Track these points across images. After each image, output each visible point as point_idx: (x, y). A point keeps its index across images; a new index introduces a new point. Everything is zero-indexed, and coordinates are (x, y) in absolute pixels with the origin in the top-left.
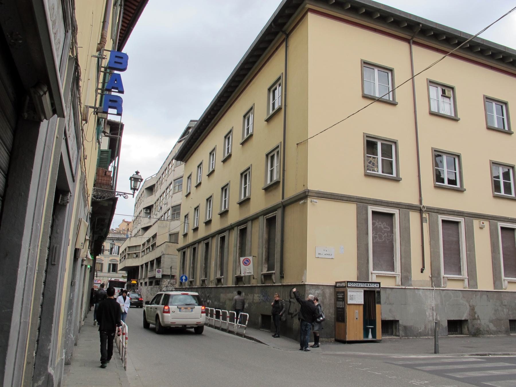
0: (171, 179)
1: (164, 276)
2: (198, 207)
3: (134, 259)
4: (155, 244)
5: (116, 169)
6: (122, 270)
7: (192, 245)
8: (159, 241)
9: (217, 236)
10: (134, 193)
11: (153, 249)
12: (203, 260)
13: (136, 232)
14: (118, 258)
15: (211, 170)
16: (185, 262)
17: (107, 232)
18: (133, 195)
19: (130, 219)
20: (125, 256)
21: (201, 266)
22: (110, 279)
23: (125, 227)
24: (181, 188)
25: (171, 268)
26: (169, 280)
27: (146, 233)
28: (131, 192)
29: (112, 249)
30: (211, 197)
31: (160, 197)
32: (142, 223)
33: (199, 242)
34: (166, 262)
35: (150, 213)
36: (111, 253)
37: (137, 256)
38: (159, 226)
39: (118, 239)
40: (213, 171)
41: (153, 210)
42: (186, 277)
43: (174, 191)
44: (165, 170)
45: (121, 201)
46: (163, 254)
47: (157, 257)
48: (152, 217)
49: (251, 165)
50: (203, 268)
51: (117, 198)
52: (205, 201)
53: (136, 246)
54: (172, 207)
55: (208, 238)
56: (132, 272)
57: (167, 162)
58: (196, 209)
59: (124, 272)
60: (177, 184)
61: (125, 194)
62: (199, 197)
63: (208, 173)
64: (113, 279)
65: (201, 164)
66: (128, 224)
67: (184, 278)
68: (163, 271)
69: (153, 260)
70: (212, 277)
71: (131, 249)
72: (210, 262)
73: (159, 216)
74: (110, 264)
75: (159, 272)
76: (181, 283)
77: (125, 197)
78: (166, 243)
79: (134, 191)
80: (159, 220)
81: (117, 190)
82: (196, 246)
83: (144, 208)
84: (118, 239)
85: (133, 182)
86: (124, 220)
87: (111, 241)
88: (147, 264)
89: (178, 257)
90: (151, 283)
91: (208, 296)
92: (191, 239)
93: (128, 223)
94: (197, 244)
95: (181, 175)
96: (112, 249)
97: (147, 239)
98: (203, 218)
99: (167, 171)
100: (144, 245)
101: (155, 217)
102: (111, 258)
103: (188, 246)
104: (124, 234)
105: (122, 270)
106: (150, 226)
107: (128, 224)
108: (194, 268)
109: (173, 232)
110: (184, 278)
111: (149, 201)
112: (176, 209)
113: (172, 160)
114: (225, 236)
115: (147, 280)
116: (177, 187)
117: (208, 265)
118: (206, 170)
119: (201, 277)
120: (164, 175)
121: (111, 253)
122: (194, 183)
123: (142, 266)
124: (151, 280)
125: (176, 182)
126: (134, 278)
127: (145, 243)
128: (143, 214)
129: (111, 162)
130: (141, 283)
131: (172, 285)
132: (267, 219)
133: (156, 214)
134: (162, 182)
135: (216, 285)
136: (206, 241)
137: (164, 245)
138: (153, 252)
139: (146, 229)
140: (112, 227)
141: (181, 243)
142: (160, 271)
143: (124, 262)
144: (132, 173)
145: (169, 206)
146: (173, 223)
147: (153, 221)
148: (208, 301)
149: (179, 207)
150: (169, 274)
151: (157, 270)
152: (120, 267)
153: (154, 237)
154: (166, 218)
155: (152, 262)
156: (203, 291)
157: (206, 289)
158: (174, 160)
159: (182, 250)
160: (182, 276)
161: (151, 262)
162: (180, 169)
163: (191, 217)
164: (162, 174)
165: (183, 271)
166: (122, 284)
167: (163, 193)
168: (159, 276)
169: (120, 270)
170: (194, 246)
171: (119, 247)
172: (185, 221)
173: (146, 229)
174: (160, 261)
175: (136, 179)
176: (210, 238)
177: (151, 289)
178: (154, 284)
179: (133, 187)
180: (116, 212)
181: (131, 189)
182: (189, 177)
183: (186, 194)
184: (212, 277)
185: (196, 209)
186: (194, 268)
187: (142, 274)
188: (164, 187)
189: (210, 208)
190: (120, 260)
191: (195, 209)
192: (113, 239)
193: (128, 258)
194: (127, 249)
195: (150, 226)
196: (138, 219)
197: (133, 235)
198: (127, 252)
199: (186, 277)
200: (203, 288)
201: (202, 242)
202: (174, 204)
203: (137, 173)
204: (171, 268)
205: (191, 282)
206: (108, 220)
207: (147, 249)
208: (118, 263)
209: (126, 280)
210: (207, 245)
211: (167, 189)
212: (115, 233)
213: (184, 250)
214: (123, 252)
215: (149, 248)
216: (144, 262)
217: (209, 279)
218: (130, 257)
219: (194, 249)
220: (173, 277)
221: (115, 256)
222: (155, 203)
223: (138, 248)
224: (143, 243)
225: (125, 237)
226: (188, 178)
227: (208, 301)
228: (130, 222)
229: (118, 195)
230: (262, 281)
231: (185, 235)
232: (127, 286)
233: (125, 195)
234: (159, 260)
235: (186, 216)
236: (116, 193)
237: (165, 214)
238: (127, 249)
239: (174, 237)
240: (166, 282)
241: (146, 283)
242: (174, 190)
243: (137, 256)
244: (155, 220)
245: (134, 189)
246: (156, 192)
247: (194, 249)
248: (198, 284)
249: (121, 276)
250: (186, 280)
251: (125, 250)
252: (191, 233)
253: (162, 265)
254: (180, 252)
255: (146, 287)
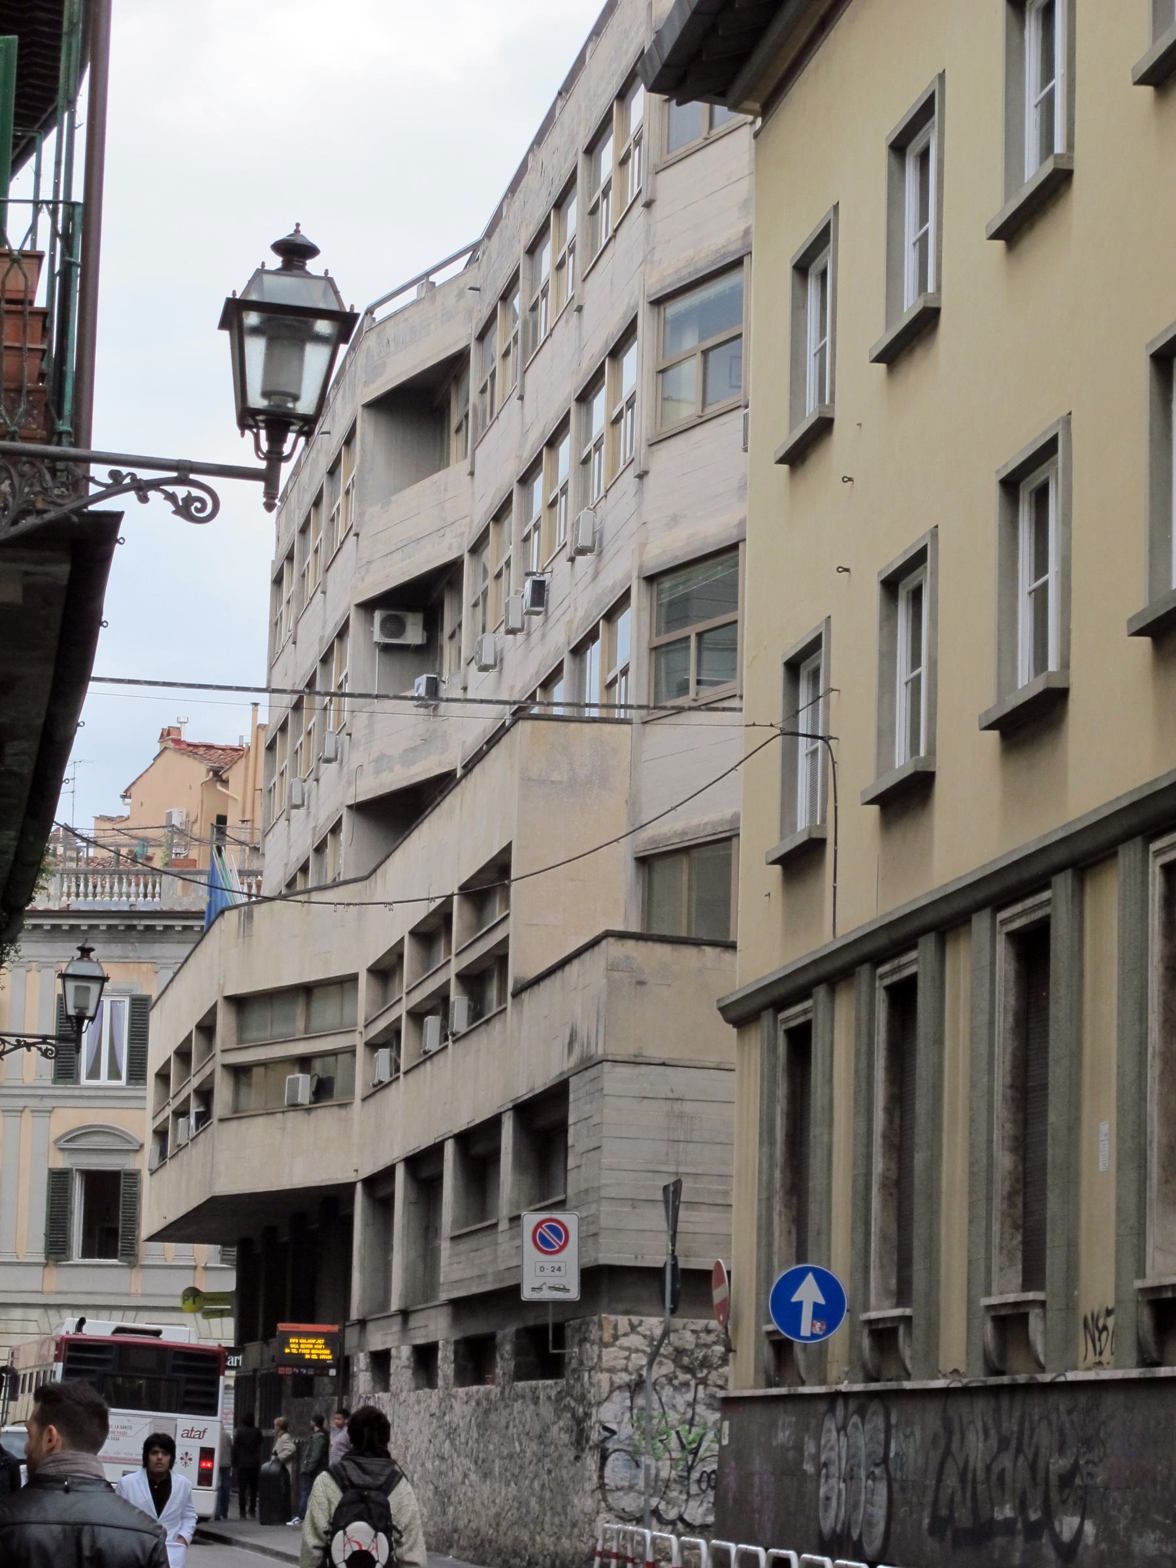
0: (617, 289)
1: (599, 1280)
2: (815, 645)
3: (295, 1119)
4: (499, 957)
5: (80, 225)
6: (181, 1230)
7: (877, 959)
8: (534, 928)
9: (1128, 855)
10: (275, 457)
11: (477, 1013)
12: (1002, 1112)
13: (303, 846)
14: (139, 1118)
15: (1033, 172)
16: (816, 1131)
17: (27, 865)
18: (269, 477)
19: (231, 723)
20: (205, 1094)
21: (981, 1172)
22: (67, 1326)
23: (184, 798)
24: (736, 381)
25: (672, 1195)
26: (653, 1324)
27: (398, 857)
28: (244, 450)
29: (72, 1026)
30: (1048, 450)
31: (526, 479)
32: (354, 758)
33: (944, 921)
34: (612, 1144)
35: (428, 651)
36: (66, 1072)
37: (323, 1091)
38: (527, 782)
39: (134, 927)
40: (1057, 184)
41: (462, 613)
42: (827, 1283)
43: (660, 415)
44: (555, 201)
45: (146, 535)
46: (589, 1064)
47: (523, 1090)
48: (445, 691)
49: (1067, 420)
50: (1001, 1187)
51: (115, 518)
52: (993, 495)
53: (306, 991)
54: (651, 579)
55: (1042, 883)
56: (287, 1250)
57: (566, 118)
58: (903, 584)
59: (207, 1253)
60: (690, 341)
61: (184, 471)
62: (922, 465)
63: (999, 210)
64: (99, 1328)
65: (926, 111)
66: (218, 776)
67: (809, 1293)
68: (590, 1236)
69: (492, 1126)
70: (1100, 1283)
71: (261, 1022)
72: (1074, 1126)
73: (520, 678)
74: (59, 1180)
75: (550, 1240)
76: (781, 1349)
77: (184, 510)
78: (610, 947)
79: (276, 439)
80: (520, 713)
81: (98, 444)
82: (1057, 898)
83: (368, 607)
84: (134, 927)
85: (256, 348)
86: (170, 738)
87: (65, 954)
88: (423, 1165)
89: (735, 1089)
90: (475, 1360)
91: (1066, 1480)
92: (862, 893)
93: (219, 764)
94: (928, 944)
95: (718, 241)
96: (72, 1026)
97: (418, 913)
98: (972, 681)
99: (573, 212)
100: (385, 971)
101: (481, 684)
102: (68, 1118)
103: (833, 973)
104: (183, 871)
105: (181, 1230)
106: (443, 784)
107: (218, 776)
108: (903, 1190)
109: (670, 829)
110: (809, 1293)
111: (411, 522)
112: (694, 596)
113: (623, 95)
114: (912, 980)
115: (437, 1328)
116: (692, 367)
117: (1054, 1153)
118: (976, 176)
119: (979, 1277)
120: (547, 257)
121: (66, 1072)
122: (865, 323)
123: (378, 1185)
124: (476, 1327)
125: (678, 325)
126: (306, 1313)
127: (395, 954)
128: (359, 662)
129: (25, 148)
130: (380, 1361)
131: (693, 1366)
132: (1012, 936)
133: (495, 655)
134: (531, 327)
135: (1145, 1362)
136: (1017, 916)
137: (593, 968)
138: (481, 1040)
139: (397, 812)
140: (64, 813)
141: (767, 940)
142: (559, 1231)
143: (195, 1153)
144: (241, 261)
145: (621, 569)
146: (667, 737)
147: (465, 727)
148: (1067, 1525)
149: (717, 571)
150: (656, 1257)
151: (531, 1219)
152: (158, 1202)
153: (490, 884)
154: (593, 694)
155: (477, 1145)
156: (1010, 1425)
157: (1053, 1398)
158: (641, 99)
159: (781, 1013)
160: (793, 1281)
161: (464, 1139)
162: (713, 182)
163: (850, 666)
164: (532, 250)
165: (799, 1220)
166: (183, 1379)
167: (552, 443)
168: (549, 1278)
169: (159, 1236)
170: (890, 962)
171: (141, 1008)
172: (793, 712)
173: (397, 812)
174: (562, 1128)
175: (280, 316)
176: (1063, 884)
177: (486, 1410)
178: (504, 1362)
179: (256, 400)
180: (107, 657)
181: (247, 418)
182: (808, 265)
183: (786, 439)
184: (1100, 1283)
185: (903, 584)
186: (903, 1190)
187: (380, 1267)
188: (552, 382)
189: (1041, 567)
190: (161, 1134)
191: (890, 585)
192: (76, 928)
193: (237, 1114)
194: (225, 1023)
195: (443, 784)
196: (311, 720)
197: (272, 882)
198: (228, 1047)
199: (827, 1283)
200: (1013, 1388)
201: (981, 923)
202: (671, 544)
203: (295, 252)
204: (672, 1195)
205: (884, 1335)
206: (31, 746)
207: (417, 1016)
208: (143, 1162)
209: (220, 1332)
210: (1032, 947)
211: (585, 397)
212: (97, 870)
213: (793, 1015)
214: (183, 1054)
215: (439, 1003)
216: (393, 1149)
217: (1071, 1305)
218: (252, 1098)
219: (903, 997)
220: (693, 1287)
221: (103, 1095)
222: (476, 549)
223: (326, 1011)
224: (375, 951)
225: (196, 899)
226: (801, 269)
227: (1067, 1525)
228: (237, 752)
229: (116, 486)
230: (1141, 1346)
231: (802, 861)
232: (243, 1386)
233: (185, 485)
234: (543, 1121)
235: (801, 666)
236: (100, 472)
237: (579, 651)
238: (225, 1023)
239: (684, 880)
240: (623, 1341)
241: (425, 1357)
242: (664, 399)
243: (323, 1091)
244: (484, 720)
245: (274, 420)
246: (483, 430)
247: (903, 997)
248: (954, 1350)
249: (174, 1296)
250: (829, 1313)
251: (206, 1028)
252: (856, 831)
253: (580, 1167)
254: (757, 1037)
255: (432, 1398)
